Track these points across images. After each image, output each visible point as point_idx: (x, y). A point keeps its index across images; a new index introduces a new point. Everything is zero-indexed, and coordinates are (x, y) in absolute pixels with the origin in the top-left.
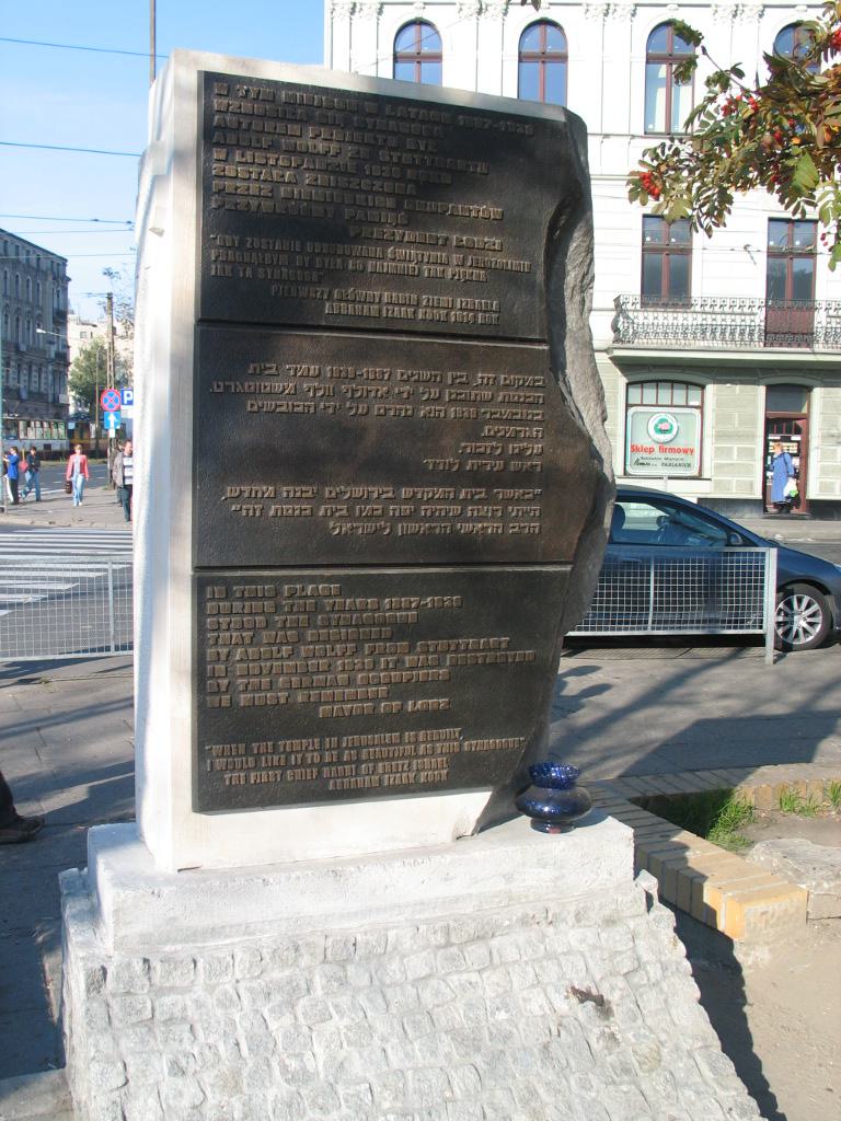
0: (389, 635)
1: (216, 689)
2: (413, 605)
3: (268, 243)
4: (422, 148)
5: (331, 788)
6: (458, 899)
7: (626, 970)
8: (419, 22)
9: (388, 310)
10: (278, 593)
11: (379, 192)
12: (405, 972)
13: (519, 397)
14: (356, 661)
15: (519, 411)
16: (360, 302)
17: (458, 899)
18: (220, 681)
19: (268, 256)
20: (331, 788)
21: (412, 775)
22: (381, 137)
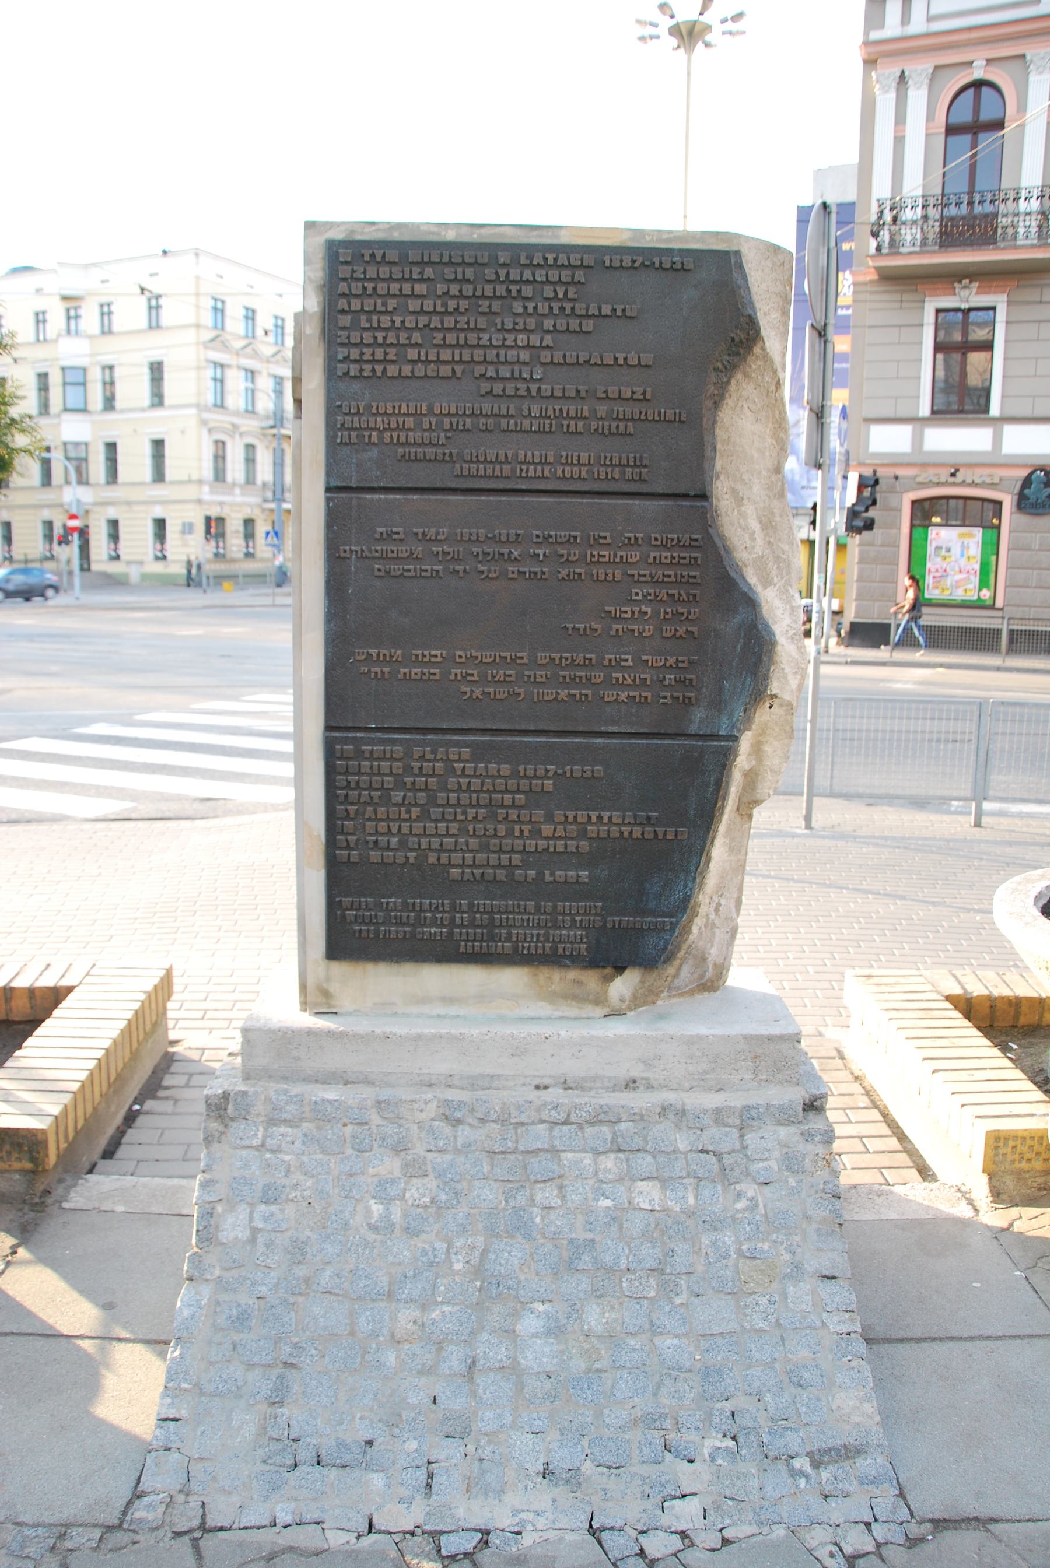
0: (523, 802)
1: (461, 862)
2: (550, 774)
3: (394, 407)
4: (561, 296)
5: (462, 950)
6: (627, 1086)
7: (565, 1128)
8: (978, 85)
9: (521, 470)
10: (408, 754)
11: (512, 347)
12: (517, 1142)
13: (673, 558)
14: (488, 826)
15: (411, 567)
16: (491, 462)
17: (627, 1086)
18: (349, 837)
19: (393, 419)
20: (462, 950)
21: (548, 945)
22: (514, 288)
